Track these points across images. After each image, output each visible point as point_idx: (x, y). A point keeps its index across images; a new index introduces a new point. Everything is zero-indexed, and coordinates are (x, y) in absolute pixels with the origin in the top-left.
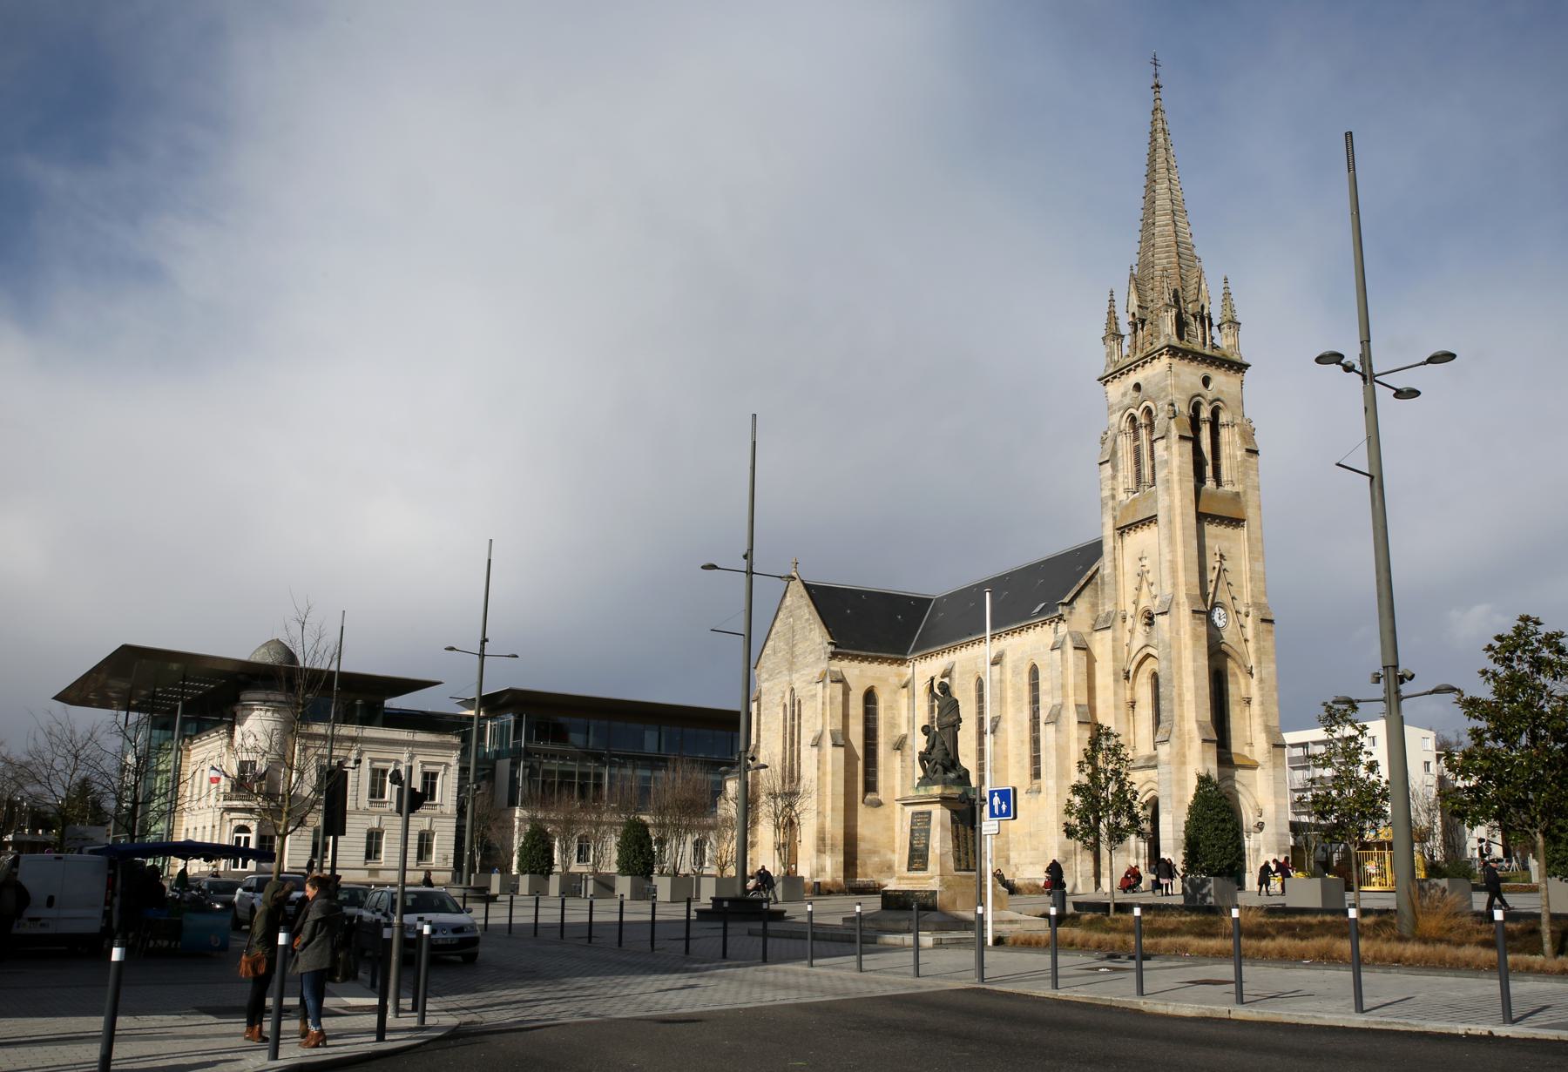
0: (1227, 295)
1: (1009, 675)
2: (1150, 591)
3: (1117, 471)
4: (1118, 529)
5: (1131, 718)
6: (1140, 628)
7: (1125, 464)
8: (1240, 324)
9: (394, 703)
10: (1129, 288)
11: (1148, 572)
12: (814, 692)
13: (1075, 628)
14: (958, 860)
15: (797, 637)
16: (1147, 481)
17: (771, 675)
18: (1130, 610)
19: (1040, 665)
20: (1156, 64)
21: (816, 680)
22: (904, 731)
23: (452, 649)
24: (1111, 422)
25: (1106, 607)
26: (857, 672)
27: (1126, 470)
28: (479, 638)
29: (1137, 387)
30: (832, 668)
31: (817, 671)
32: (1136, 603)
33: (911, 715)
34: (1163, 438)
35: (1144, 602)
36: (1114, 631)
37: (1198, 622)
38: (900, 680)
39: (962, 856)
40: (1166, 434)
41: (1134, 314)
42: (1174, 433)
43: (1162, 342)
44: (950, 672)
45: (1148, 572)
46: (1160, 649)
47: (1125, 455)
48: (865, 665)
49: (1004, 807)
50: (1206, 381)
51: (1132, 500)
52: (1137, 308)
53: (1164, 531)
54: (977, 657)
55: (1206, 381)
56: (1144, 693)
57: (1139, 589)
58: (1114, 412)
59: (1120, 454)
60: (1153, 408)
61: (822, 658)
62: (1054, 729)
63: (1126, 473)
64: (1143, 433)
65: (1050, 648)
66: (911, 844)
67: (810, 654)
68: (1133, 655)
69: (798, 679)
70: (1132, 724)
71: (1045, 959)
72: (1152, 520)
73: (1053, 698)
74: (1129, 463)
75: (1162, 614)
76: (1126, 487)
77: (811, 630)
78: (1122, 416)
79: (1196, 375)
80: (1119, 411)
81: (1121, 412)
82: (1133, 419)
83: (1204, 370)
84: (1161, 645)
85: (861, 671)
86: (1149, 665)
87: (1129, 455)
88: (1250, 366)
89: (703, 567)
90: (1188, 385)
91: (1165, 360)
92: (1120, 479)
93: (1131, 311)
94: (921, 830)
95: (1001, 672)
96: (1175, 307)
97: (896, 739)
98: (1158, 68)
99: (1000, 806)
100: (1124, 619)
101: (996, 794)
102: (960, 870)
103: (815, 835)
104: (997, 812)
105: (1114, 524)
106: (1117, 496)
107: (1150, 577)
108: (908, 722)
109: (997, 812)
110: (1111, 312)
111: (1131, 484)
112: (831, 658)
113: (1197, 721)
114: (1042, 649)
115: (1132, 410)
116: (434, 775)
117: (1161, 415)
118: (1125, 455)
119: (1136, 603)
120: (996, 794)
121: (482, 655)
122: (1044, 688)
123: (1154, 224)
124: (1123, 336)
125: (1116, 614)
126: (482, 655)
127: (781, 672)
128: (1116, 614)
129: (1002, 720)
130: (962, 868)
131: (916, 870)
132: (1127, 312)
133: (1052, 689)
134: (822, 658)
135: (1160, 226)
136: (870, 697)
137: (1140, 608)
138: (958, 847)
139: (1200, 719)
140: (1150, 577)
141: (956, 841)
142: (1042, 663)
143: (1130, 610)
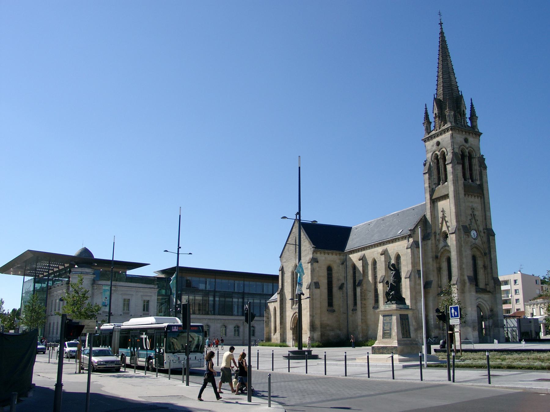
0: (472, 106)
5: (439, 275)
7: (434, 173)
8: (478, 117)
9: (130, 272)
10: (434, 103)
17: (287, 260)
19: (402, 255)
20: (440, 15)
21: (307, 262)
22: (343, 281)
23: (190, 254)
24: (427, 157)
25: (428, 231)
26: (323, 258)
27: (434, 176)
28: (177, 247)
33: (346, 275)
37: (467, 236)
41: (436, 114)
49: (456, 313)
50: (466, 141)
58: (429, 153)
61: (310, 253)
62: (409, 280)
66: (383, 328)
70: (439, 277)
71: (485, 372)
73: (408, 268)
79: (462, 138)
81: (432, 153)
85: (325, 258)
88: (482, 134)
89: (281, 218)
93: (435, 112)
98: (441, 16)
99: (454, 313)
101: (453, 308)
102: (404, 338)
103: (309, 324)
104: (453, 315)
109: (453, 315)
110: (426, 113)
113: (467, 276)
116: (148, 302)
120: (453, 308)
121: (178, 254)
122: (403, 264)
124: (431, 122)
126: (178, 254)
127: (291, 259)
130: (405, 337)
132: (433, 113)
133: (407, 264)
134: (310, 253)
138: (403, 329)
139: (469, 275)
142: (402, 253)
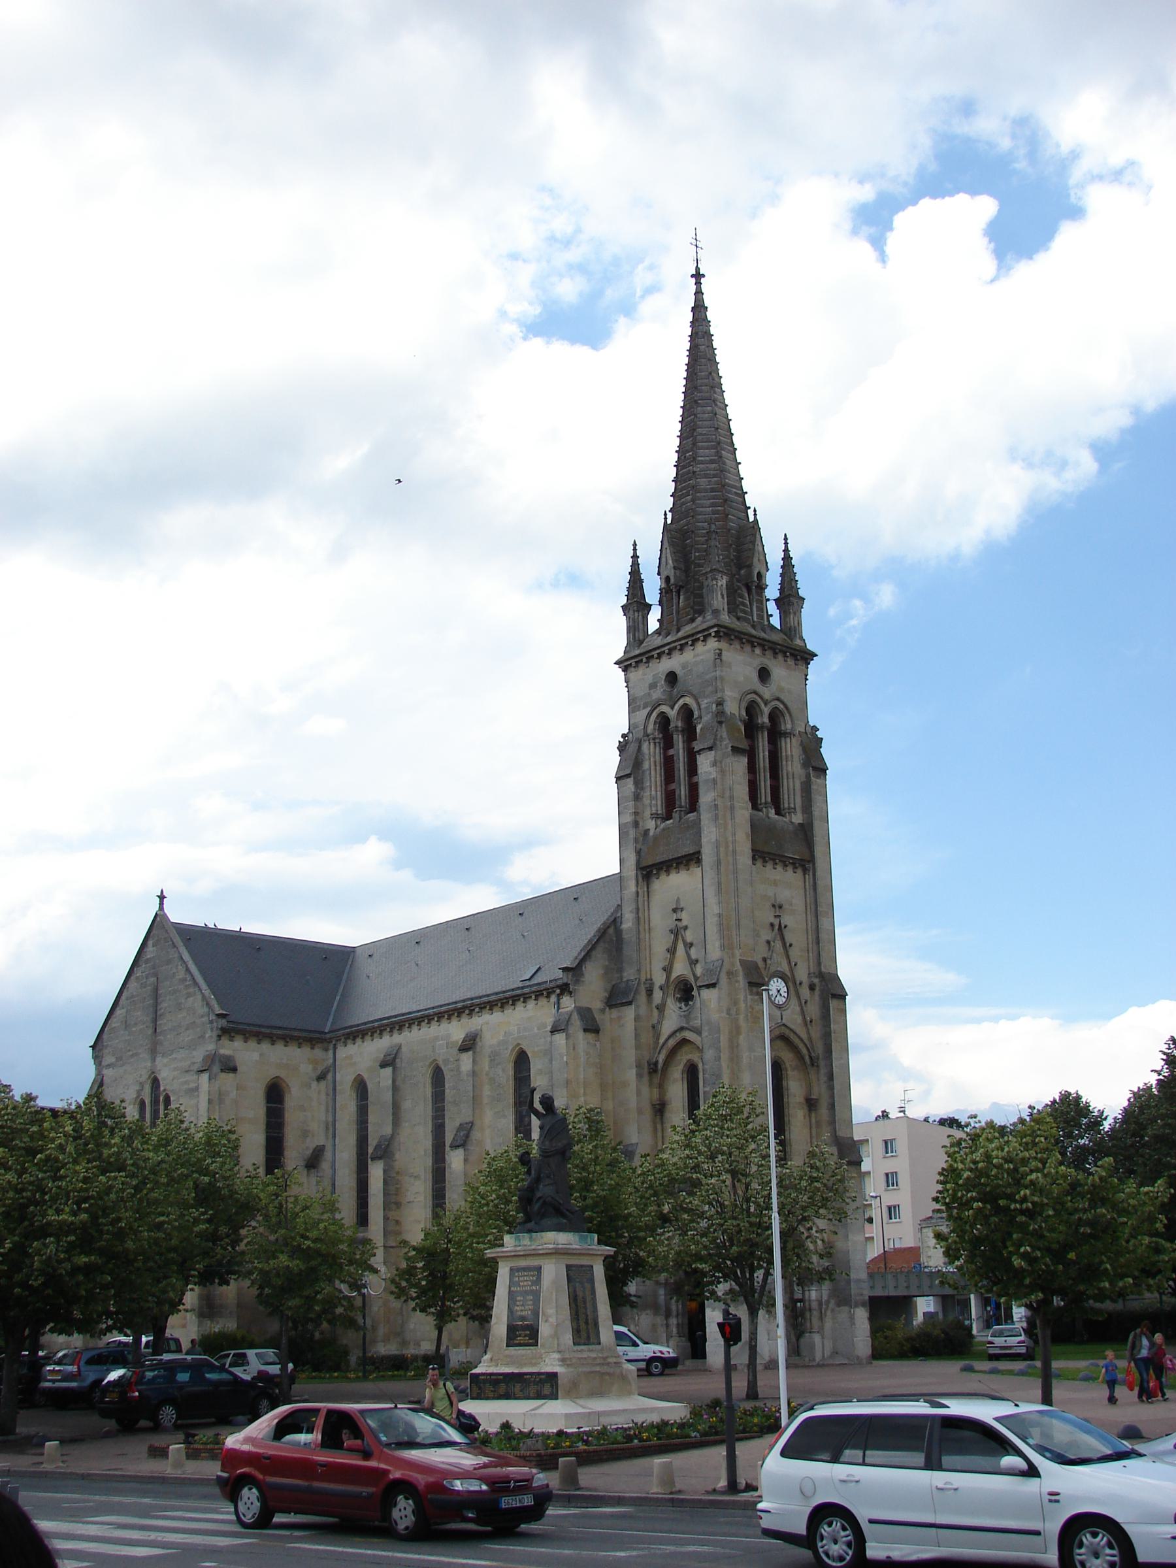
1: (485, 1064)
2: (688, 955)
3: (642, 789)
4: (643, 869)
5: (659, 1127)
6: (673, 1007)
11: (686, 928)
12: (193, 1085)
13: (584, 1003)
14: (577, 1332)
15: (164, 1005)
16: (683, 804)
17: (119, 1059)
18: (659, 978)
21: (196, 1067)
25: (625, 974)
29: (672, 678)
30: (222, 1051)
31: (198, 1056)
32: (668, 969)
33: (330, 1119)
34: (710, 749)
35: (680, 969)
36: (637, 1007)
38: (315, 1069)
39: (583, 1326)
40: (715, 744)
42: (726, 744)
43: (707, 620)
44: (394, 1059)
45: (686, 928)
46: (705, 1034)
47: (653, 768)
48: (265, 1046)
50: (764, 674)
51: (664, 830)
52: (673, 571)
53: (710, 875)
54: (436, 1038)
55: (764, 674)
56: (677, 1092)
57: (672, 951)
59: (646, 765)
60: (694, 706)
63: (653, 793)
64: (679, 741)
65: (549, 1028)
67: (187, 1029)
68: (662, 1041)
69: (165, 1065)
70: (659, 1134)
72: (693, 859)
74: (658, 779)
75: (708, 986)
76: (654, 812)
77: (189, 995)
78: (649, 715)
80: (644, 708)
82: (664, 721)
83: (758, 659)
84: (706, 1028)
86: (684, 1057)
87: (658, 768)
90: (741, 679)
91: (712, 644)
92: (647, 801)
94: (526, 1293)
95: (474, 1061)
96: (726, 574)
97: (309, 1152)
100: (650, 992)
102: (579, 1344)
105: (638, 862)
106: (641, 823)
107: (689, 936)
108: (327, 1128)
111: (659, 806)
112: (219, 1037)
114: (536, 1030)
115: (665, 708)
117: (706, 718)
118: (653, 768)
119: (668, 969)
123: (694, 459)
125: (639, 984)
127: (137, 1054)
128: (639, 984)
129: (475, 1128)
131: (520, 1345)
135: (702, 462)
136: (275, 1094)
137: (674, 975)
140: (689, 936)
141: (573, 1306)
143: (659, 978)
